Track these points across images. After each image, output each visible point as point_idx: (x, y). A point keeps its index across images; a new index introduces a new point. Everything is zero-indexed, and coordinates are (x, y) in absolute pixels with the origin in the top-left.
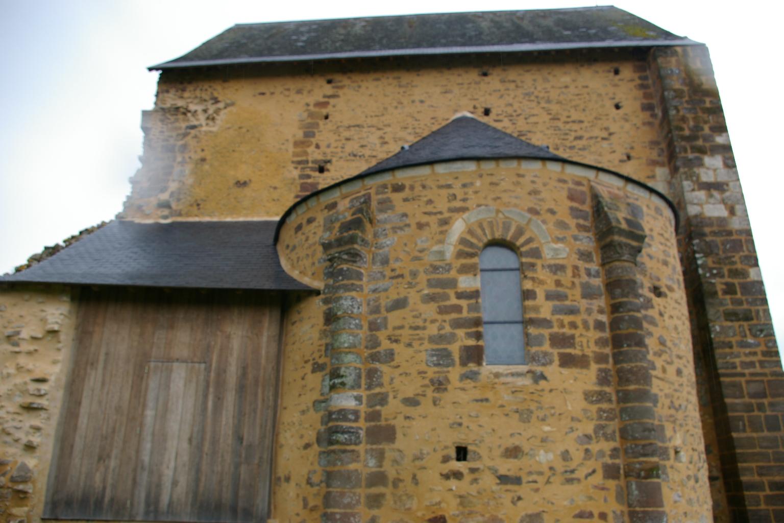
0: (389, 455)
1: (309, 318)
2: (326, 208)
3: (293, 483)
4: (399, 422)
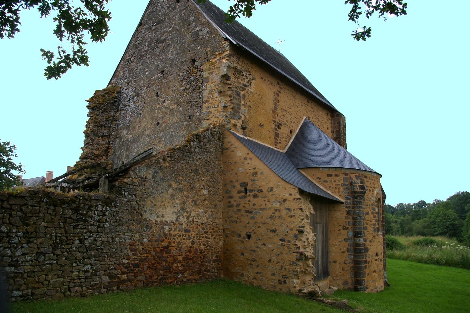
0: (368, 255)
1: (339, 211)
2: (344, 174)
3: (337, 263)
4: (369, 247)
